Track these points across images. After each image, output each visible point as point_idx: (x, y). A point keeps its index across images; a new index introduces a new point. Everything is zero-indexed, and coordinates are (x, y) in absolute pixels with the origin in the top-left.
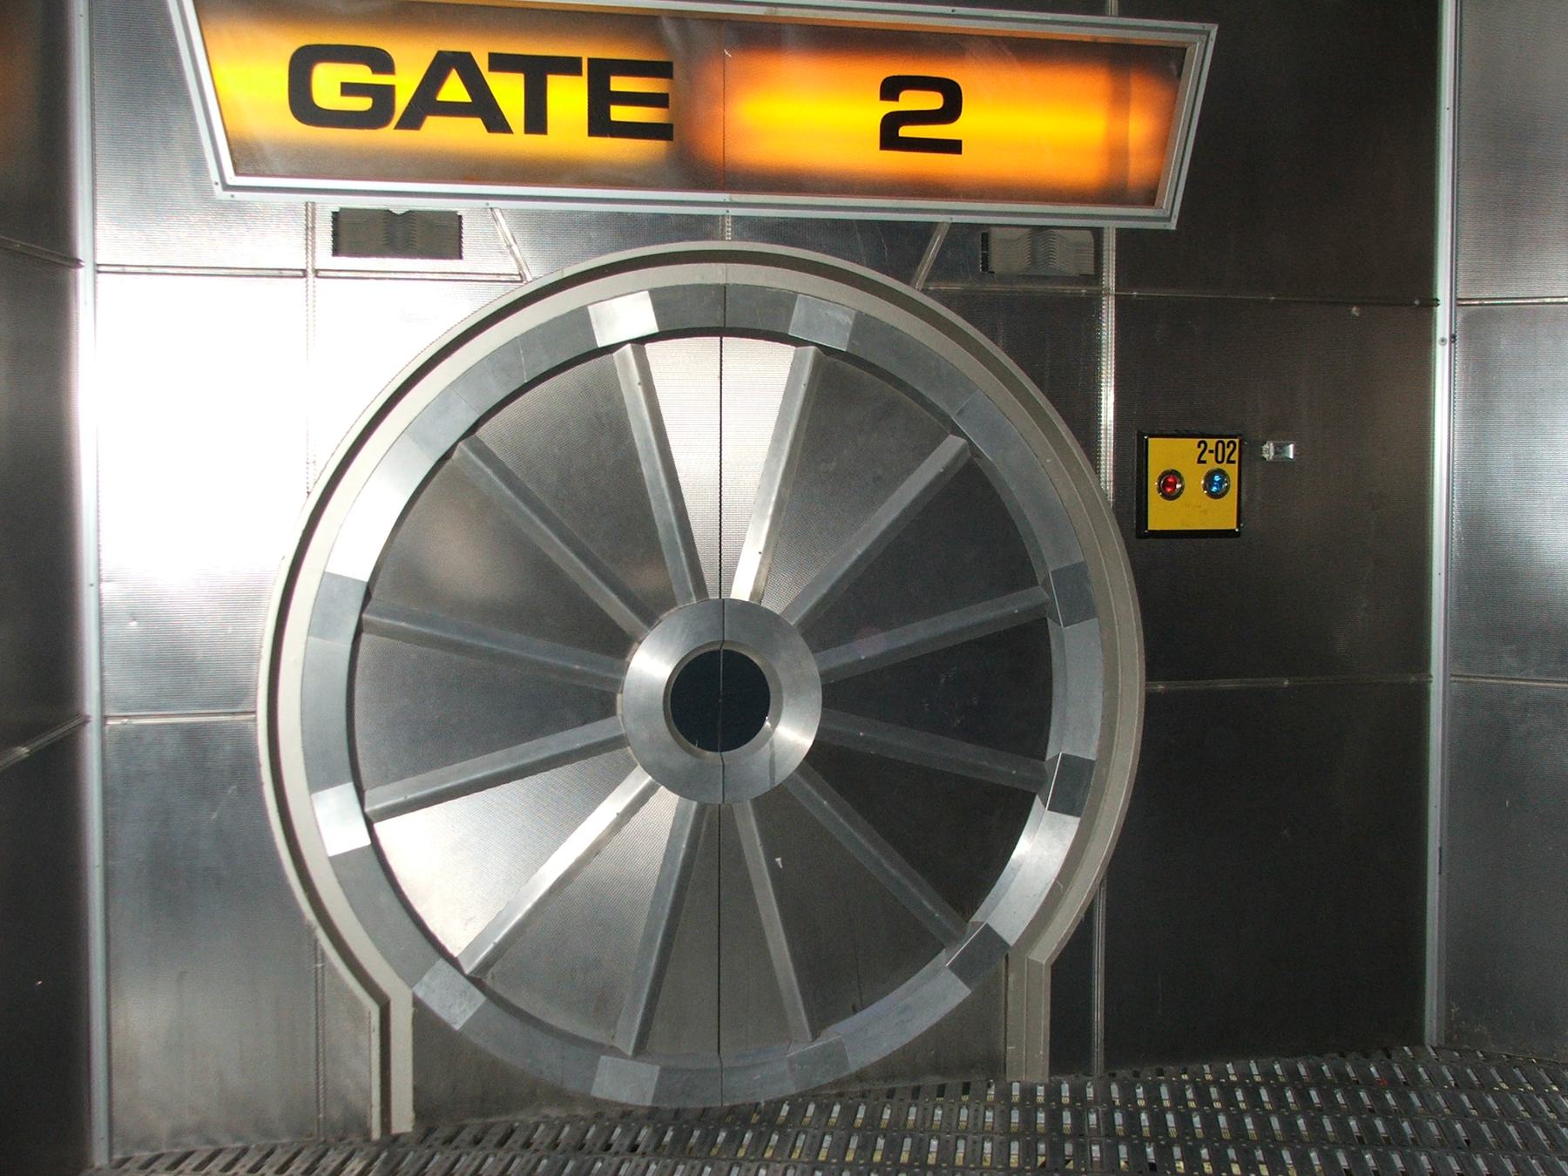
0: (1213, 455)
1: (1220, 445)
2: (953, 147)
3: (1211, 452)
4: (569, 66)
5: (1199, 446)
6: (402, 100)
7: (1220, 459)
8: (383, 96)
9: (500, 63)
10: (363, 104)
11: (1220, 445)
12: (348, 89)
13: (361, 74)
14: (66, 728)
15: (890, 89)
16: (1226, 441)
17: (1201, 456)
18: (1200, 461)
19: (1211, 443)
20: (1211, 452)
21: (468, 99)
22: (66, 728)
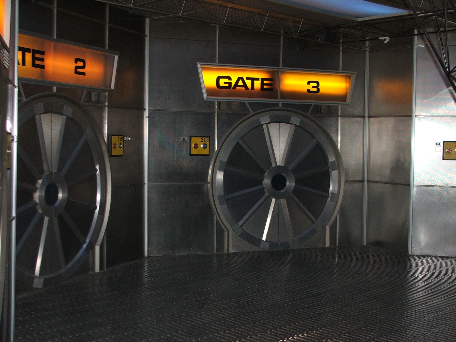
0: (204, 141)
1: (205, 139)
2: (84, 74)
3: (204, 140)
4: (258, 79)
5: (202, 139)
6: (233, 85)
7: (205, 141)
8: (230, 84)
9: (248, 79)
10: (227, 85)
11: (205, 139)
12: (225, 83)
13: (227, 80)
14: (202, 183)
15: (77, 60)
16: (206, 138)
17: (202, 140)
18: (202, 141)
19: (204, 138)
20: (204, 140)
21: (243, 84)
22: (202, 183)
